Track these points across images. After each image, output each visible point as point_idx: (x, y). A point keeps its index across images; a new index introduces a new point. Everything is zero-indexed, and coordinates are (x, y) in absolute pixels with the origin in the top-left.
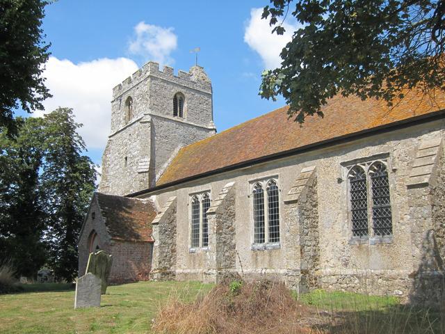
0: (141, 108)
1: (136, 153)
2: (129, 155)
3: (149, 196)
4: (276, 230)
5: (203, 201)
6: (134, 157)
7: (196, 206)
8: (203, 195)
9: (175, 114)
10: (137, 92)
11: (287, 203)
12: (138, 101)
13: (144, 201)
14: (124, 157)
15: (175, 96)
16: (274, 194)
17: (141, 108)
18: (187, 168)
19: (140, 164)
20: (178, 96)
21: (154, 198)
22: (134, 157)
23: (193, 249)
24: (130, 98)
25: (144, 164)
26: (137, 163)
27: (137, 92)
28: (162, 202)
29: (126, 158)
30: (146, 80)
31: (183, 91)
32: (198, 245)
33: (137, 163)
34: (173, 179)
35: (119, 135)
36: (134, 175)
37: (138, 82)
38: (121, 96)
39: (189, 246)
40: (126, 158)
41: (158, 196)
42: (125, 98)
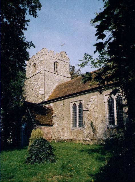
0: (40, 68)
1: (37, 87)
2: (34, 88)
3: (49, 103)
4: (112, 117)
5: (78, 105)
6: (37, 88)
7: (74, 108)
8: (73, 103)
9: (54, 71)
10: (38, 61)
11: (84, 111)
12: (38, 65)
13: (47, 106)
14: (32, 89)
16: (81, 106)
17: (40, 68)
18: (61, 93)
19: (40, 91)
21: (51, 105)
22: (37, 88)
23: (74, 128)
24: (35, 64)
26: (38, 91)
27: (38, 61)
28: (55, 106)
29: (33, 89)
31: (58, 61)
32: (76, 126)
33: (38, 91)
34: (55, 98)
36: (36, 96)
37: (38, 57)
38: (31, 63)
39: (71, 127)
40: (33, 89)
41: (53, 103)
42: (33, 63)
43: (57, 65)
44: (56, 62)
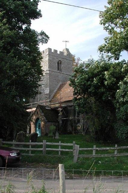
9: (58, 70)
15: (58, 62)
20: (59, 62)
25: (47, 91)
30: (46, 56)
43: (60, 63)
44: (60, 61)
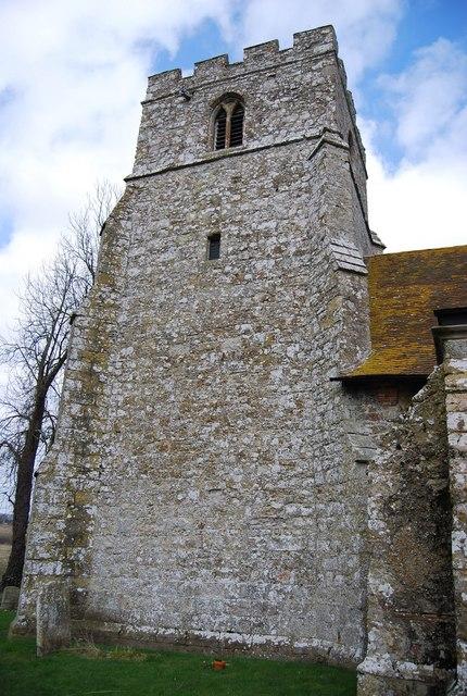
35: (179, 176)
